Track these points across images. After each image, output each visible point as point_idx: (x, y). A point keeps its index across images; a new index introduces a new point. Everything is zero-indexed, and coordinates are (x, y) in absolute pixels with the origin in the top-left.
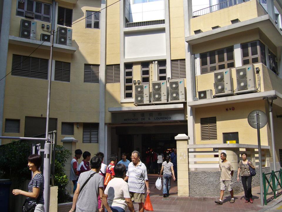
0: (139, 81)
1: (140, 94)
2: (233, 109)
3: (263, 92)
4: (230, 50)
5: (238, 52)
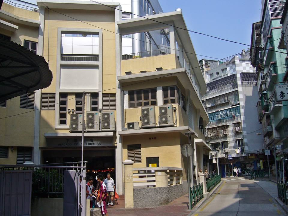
0: (73, 110)
1: (75, 122)
2: (155, 138)
3: (179, 127)
4: (154, 91)
5: (160, 94)
